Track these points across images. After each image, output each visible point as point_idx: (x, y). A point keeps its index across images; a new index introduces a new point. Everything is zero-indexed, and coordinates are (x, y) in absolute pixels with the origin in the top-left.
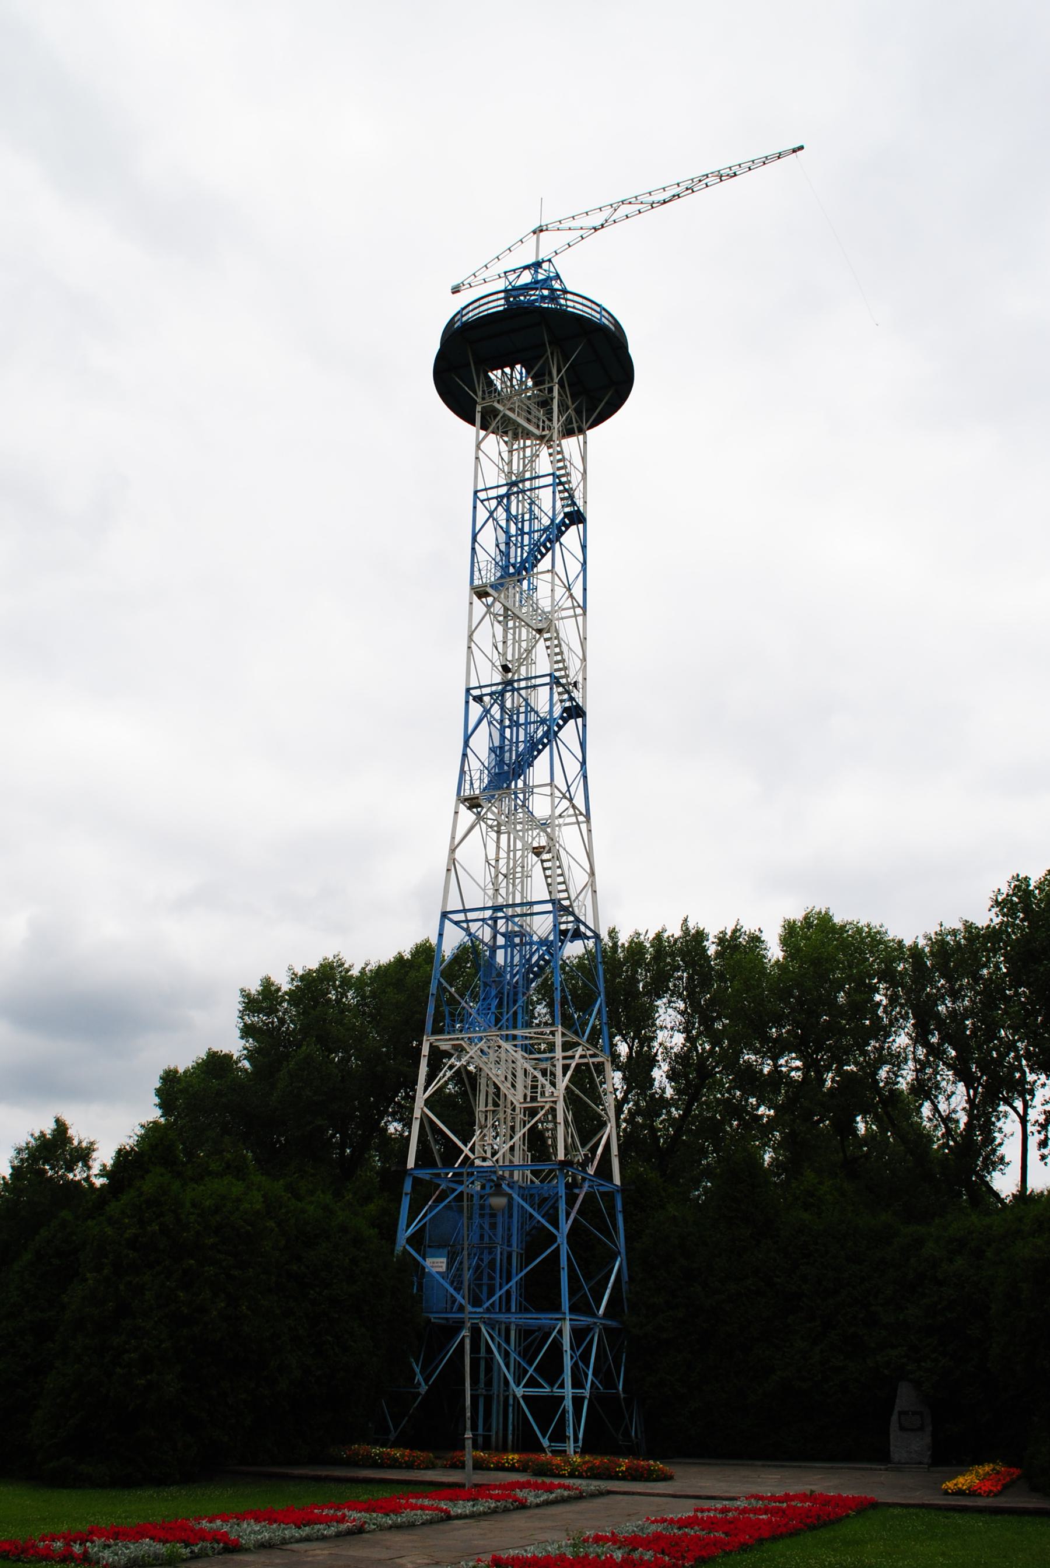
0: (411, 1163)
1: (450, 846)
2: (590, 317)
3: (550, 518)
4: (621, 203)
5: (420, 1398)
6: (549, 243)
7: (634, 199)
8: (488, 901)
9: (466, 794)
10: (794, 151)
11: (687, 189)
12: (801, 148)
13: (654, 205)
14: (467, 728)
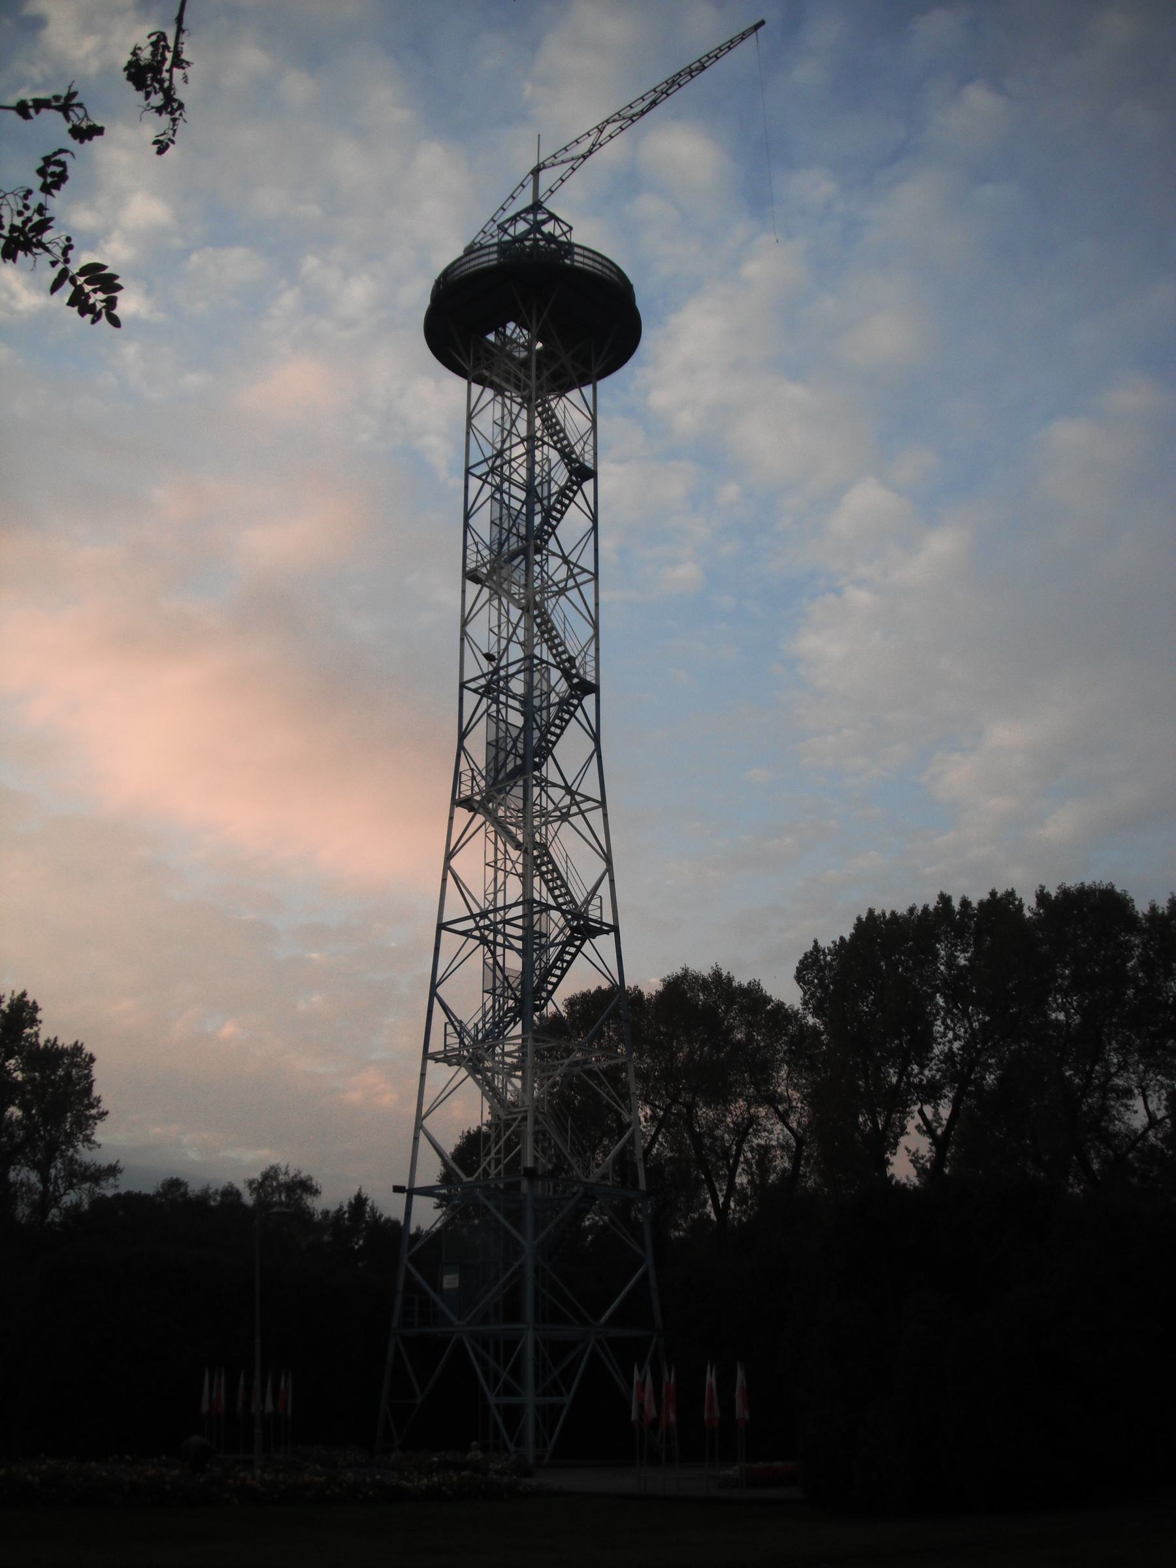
1: (446, 854)
2: (600, 273)
3: (561, 824)
4: (605, 123)
5: (565, 1412)
6: (547, 178)
7: (617, 116)
8: (495, 544)
9: (462, 796)
10: (756, 28)
11: (662, 93)
12: (762, 23)
13: (634, 118)
14: (436, 976)
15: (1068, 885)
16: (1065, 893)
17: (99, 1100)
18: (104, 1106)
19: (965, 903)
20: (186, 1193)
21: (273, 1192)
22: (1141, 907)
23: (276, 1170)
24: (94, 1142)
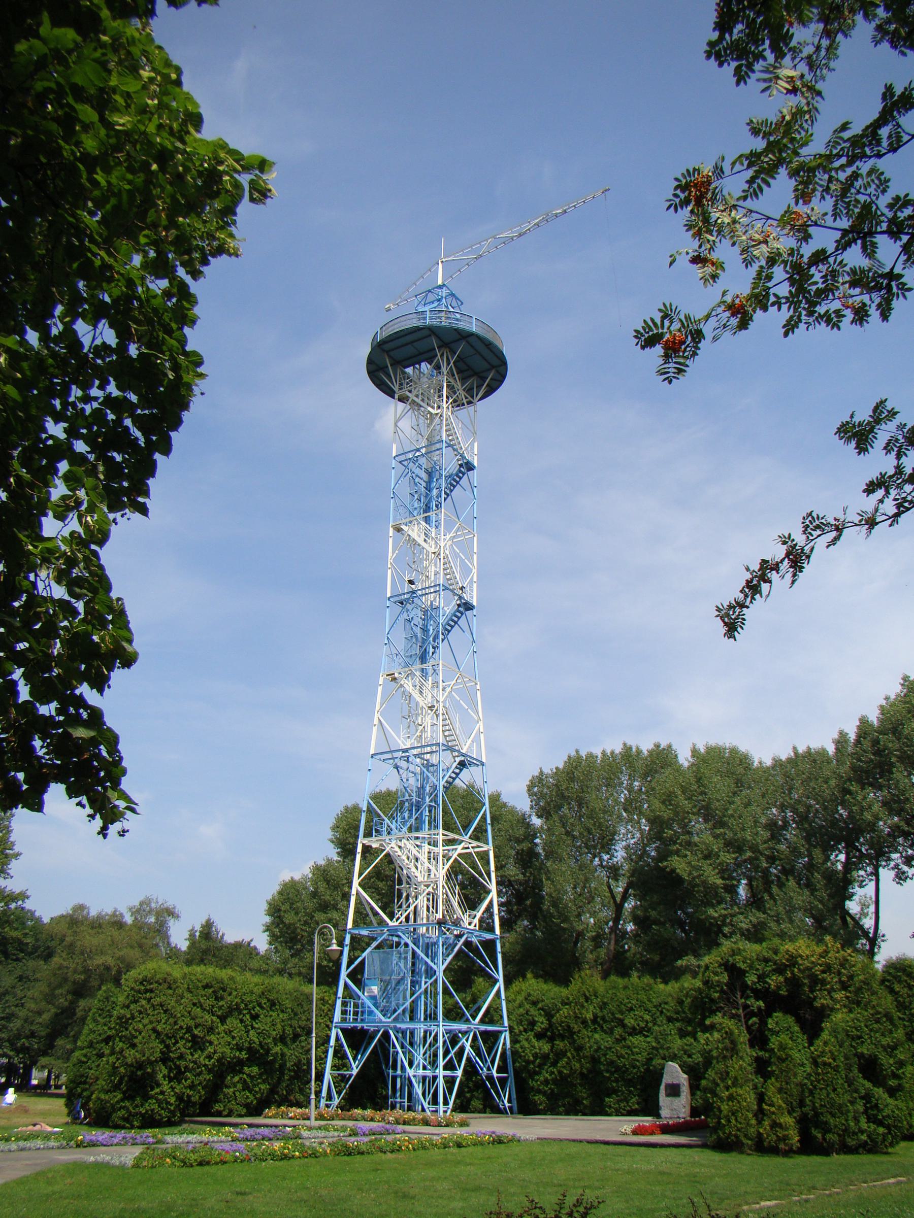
0: (350, 925)
15: (710, 743)
16: (710, 750)
17: (13, 844)
18: (17, 849)
19: (612, 753)
20: (273, 923)
21: (532, 932)
22: (63, 786)
23: (335, 907)
24: (8, 874)
